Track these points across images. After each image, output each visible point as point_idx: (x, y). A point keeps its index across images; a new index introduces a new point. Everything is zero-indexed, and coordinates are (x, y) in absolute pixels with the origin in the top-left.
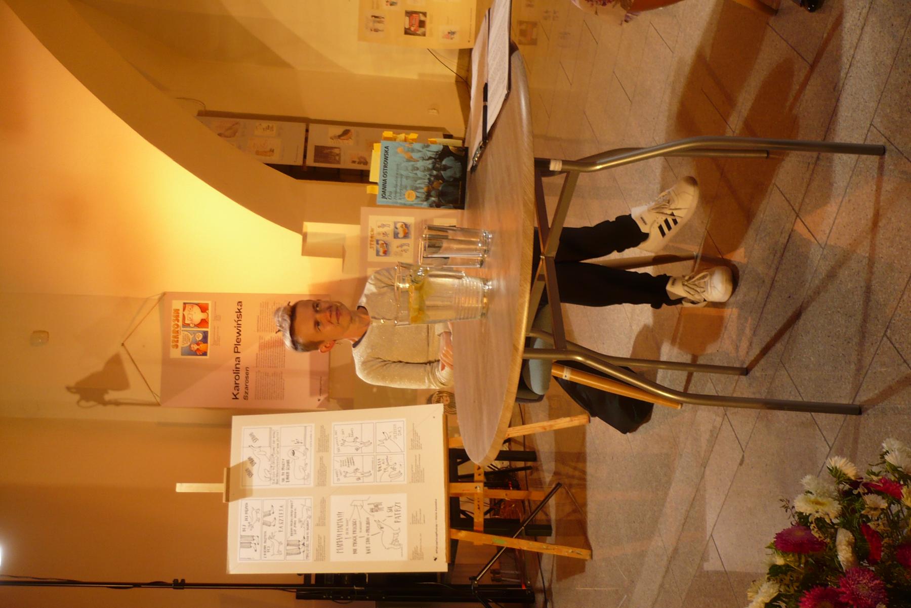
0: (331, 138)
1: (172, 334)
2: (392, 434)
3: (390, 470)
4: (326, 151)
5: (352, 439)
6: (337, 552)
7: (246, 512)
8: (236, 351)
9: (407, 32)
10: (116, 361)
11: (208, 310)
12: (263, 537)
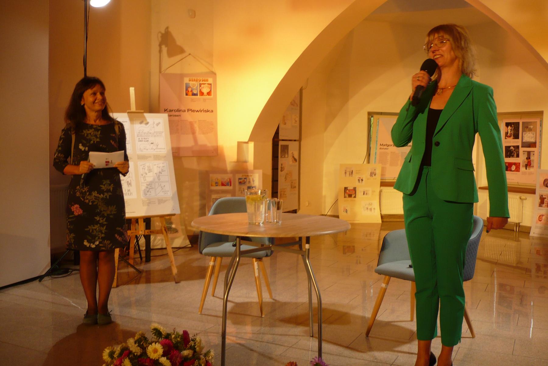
0: (292, 153)
1: (196, 78)
2: (164, 190)
3: (148, 190)
4: (286, 150)
9: (346, 189)
10: (182, 51)
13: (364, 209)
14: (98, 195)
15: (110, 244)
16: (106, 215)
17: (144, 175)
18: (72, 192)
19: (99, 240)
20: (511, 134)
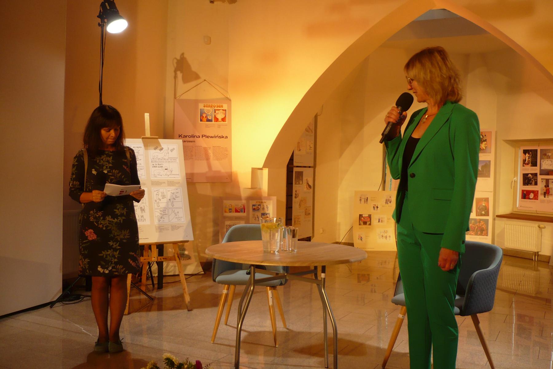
1: (210, 104)
2: (178, 216)
5: (174, 197)
8: (203, 136)
9: (361, 216)
10: (197, 77)
11: (223, 122)
13: (379, 237)
17: (158, 201)
20: (529, 161)
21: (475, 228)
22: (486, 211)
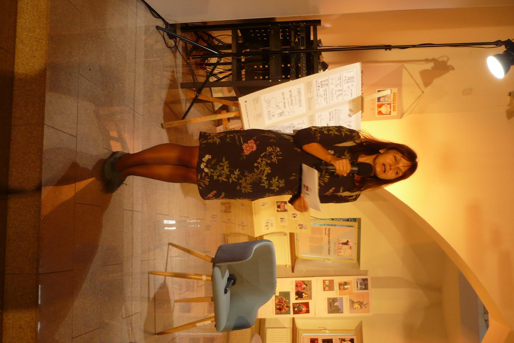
6: (300, 88)
7: (352, 93)
11: (378, 113)
12: (342, 84)
14: (266, 174)
15: (204, 184)
16: (240, 181)
18: (272, 140)
19: (210, 173)
21: (282, 303)
22: (298, 311)
